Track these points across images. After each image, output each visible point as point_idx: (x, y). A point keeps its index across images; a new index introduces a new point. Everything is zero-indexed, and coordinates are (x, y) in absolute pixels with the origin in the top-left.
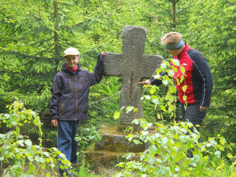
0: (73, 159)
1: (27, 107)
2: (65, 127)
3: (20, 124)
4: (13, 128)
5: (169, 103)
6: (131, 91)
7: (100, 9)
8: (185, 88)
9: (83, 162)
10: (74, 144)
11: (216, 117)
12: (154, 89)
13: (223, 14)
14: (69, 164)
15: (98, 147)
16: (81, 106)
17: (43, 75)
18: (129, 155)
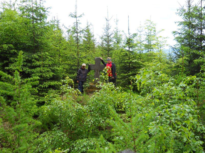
0: (82, 92)
1: (70, 78)
2: (80, 82)
3: (68, 83)
4: (66, 84)
5: (107, 78)
6: (97, 74)
7: (89, 53)
8: (111, 74)
9: (85, 92)
10: (83, 87)
11: (119, 81)
12: (103, 74)
13: (121, 54)
14: (81, 93)
15: (89, 88)
16: (85, 78)
17: (75, 70)
18: (96, 91)
